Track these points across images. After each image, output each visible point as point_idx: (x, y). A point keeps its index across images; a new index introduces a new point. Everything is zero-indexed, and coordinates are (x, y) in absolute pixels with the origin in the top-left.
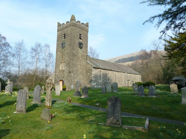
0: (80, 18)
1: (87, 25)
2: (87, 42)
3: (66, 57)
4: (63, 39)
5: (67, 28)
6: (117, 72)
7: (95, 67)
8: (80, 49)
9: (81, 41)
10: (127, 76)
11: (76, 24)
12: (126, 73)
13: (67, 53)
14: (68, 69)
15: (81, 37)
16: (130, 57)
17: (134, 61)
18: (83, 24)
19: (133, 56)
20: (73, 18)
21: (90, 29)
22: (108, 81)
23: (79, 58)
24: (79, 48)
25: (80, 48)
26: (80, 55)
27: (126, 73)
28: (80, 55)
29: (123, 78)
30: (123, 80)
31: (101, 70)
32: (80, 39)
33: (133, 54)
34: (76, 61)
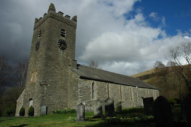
0: (66, 9)
1: (75, 19)
2: (75, 41)
3: (39, 63)
4: (39, 38)
5: (44, 23)
6: (123, 85)
7: (84, 75)
8: (62, 51)
9: (64, 39)
10: (139, 91)
11: (55, 16)
12: (137, 87)
13: (41, 56)
14: (39, 81)
15: (64, 33)
16: (145, 75)
17: (150, 78)
18: (68, 16)
19: (148, 73)
20: (52, 8)
21: (78, 23)
22: (131, 100)
23: (58, 64)
24: (59, 49)
25: (61, 49)
26: (61, 59)
27: (137, 87)
28: (61, 59)
29: (133, 94)
30: (133, 97)
31: (94, 81)
32: (63, 36)
33: (148, 71)
34: (53, 67)
